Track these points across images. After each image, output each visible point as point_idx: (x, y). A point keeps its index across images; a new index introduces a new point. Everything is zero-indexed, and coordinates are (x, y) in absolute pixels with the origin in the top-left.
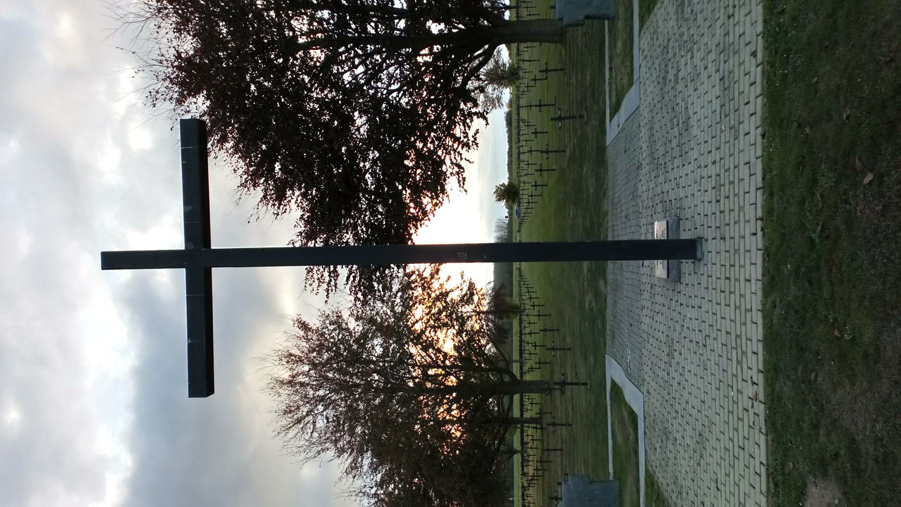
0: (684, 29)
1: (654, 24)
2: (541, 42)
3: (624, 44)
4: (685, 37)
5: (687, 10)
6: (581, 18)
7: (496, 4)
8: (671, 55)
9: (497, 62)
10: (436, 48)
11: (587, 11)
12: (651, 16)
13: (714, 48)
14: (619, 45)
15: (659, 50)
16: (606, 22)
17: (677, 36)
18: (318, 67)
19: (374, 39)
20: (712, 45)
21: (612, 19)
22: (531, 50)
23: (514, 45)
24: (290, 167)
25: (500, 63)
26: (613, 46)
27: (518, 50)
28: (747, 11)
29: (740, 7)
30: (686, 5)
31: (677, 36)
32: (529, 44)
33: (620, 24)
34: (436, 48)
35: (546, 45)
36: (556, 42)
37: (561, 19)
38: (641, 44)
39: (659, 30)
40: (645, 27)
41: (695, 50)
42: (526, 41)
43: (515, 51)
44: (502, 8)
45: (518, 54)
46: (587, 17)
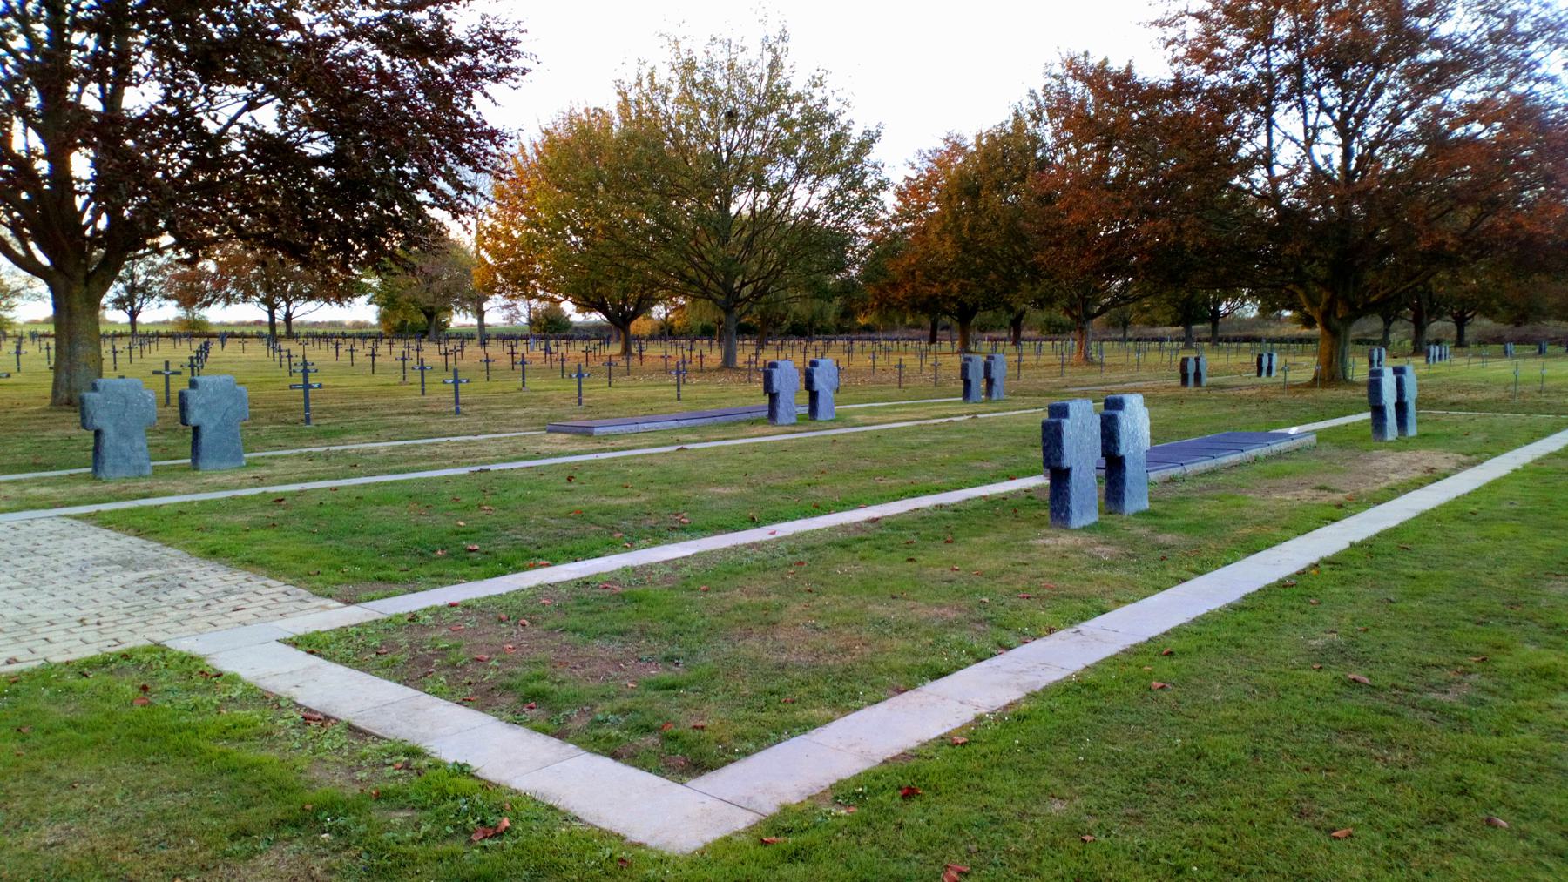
0: (66, 570)
1: (80, 533)
2: (56, 369)
3: (45, 497)
4: (50, 575)
5: (100, 571)
6: (97, 423)
7: (140, 295)
8: (19, 561)
9: (16, 293)
10: (42, 167)
11: (110, 433)
12: (94, 528)
13: (27, 612)
14: (44, 491)
15: (28, 545)
16: (90, 469)
17: (55, 564)
18: (415, 188)
19: (60, 44)
20: (34, 609)
21: (95, 476)
22: (39, 357)
23: (51, 329)
24: (854, 272)
25: (15, 300)
26: (41, 483)
27: (45, 336)
28: (89, 640)
29: (98, 631)
30: (108, 568)
31: (55, 564)
32: (52, 352)
33: (84, 488)
34: (42, 167)
35: (51, 375)
36: (55, 393)
37: (94, 388)
38: (44, 521)
39: (66, 541)
40: (74, 522)
41: (25, 590)
42: (58, 348)
43: (41, 330)
44: (132, 305)
45: (34, 336)
46: (98, 433)
